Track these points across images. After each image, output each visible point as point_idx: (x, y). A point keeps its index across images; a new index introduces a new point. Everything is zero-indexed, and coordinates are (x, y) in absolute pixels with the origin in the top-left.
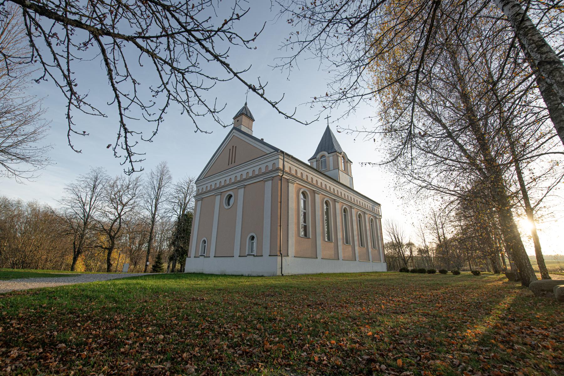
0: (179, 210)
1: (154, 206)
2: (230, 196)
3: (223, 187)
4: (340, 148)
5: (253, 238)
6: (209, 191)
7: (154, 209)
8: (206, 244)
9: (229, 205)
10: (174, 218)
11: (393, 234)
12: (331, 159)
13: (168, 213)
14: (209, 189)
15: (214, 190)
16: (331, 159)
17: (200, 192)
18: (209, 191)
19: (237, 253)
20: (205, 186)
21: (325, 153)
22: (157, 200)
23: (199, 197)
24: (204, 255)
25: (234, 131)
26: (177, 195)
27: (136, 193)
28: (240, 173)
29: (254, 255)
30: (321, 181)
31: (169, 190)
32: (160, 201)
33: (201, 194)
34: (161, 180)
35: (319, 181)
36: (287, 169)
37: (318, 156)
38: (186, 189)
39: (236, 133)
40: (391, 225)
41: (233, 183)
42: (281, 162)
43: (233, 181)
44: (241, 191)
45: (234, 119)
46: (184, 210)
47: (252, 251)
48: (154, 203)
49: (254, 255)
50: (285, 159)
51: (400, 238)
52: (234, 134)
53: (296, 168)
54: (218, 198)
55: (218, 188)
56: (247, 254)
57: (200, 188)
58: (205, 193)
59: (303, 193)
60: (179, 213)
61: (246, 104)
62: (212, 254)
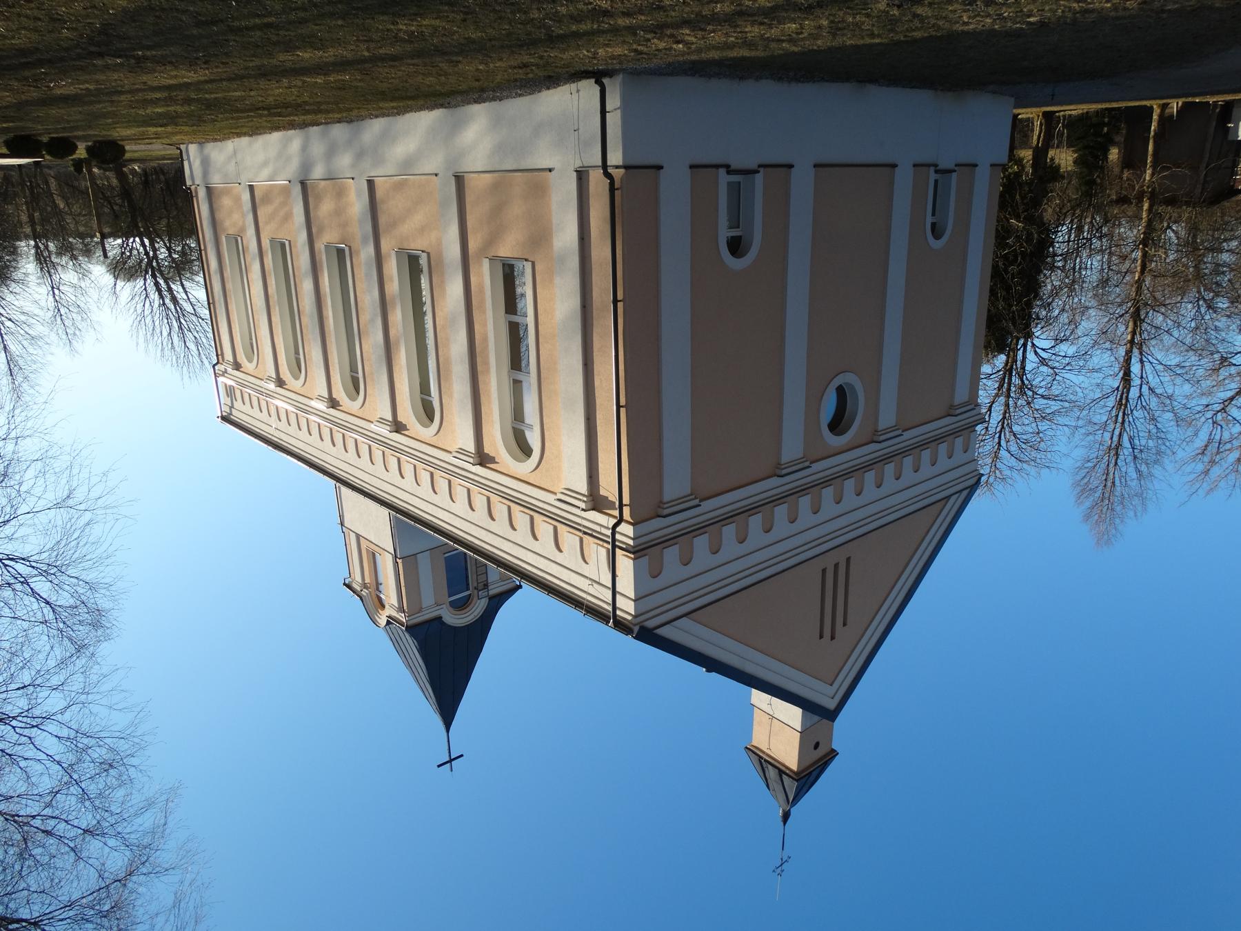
0: (1029, 367)
1: (1136, 381)
2: (837, 425)
3: (867, 466)
4: (396, 642)
5: (736, 247)
6: (923, 445)
7: (1135, 368)
8: (929, 220)
9: (841, 391)
10: (1042, 339)
11: (180, 313)
12: (436, 604)
13: (1073, 354)
14: (943, 448)
15: (904, 453)
16: (436, 604)
17: (959, 442)
18: (923, 445)
19: (803, 183)
20: (885, 490)
21: (454, 619)
22: (1122, 404)
23: (965, 419)
24: (939, 177)
25: (831, 705)
26: (1043, 426)
27: (1208, 427)
28: (885, 490)
29: (730, 171)
30: (454, 508)
31: (1069, 447)
32: (1111, 402)
33: (955, 433)
34: (1108, 484)
35: (460, 506)
36: (598, 553)
37: (478, 607)
38: (1003, 453)
39: (825, 696)
40: (192, 346)
41: (826, 482)
42: (626, 584)
43: (828, 493)
44: (792, 449)
45: (833, 754)
46: (1008, 370)
47: (735, 190)
48: (1134, 393)
49: (730, 171)
50: (608, 595)
51: (154, 296)
52: (831, 690)
53: (559, 557)
54: (887, 418)
55: (887, 459)
56: (759, 178)
57: (959, 457)
58: (939, 439)
59: (526, 451)
60: (1031, 356)
61: (786, 817)
62: (904, 179)
